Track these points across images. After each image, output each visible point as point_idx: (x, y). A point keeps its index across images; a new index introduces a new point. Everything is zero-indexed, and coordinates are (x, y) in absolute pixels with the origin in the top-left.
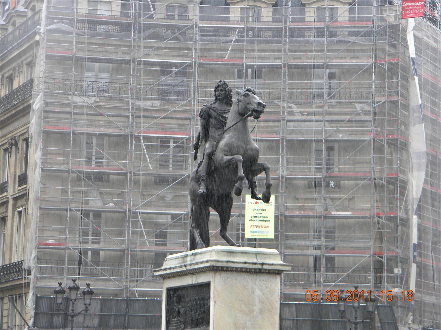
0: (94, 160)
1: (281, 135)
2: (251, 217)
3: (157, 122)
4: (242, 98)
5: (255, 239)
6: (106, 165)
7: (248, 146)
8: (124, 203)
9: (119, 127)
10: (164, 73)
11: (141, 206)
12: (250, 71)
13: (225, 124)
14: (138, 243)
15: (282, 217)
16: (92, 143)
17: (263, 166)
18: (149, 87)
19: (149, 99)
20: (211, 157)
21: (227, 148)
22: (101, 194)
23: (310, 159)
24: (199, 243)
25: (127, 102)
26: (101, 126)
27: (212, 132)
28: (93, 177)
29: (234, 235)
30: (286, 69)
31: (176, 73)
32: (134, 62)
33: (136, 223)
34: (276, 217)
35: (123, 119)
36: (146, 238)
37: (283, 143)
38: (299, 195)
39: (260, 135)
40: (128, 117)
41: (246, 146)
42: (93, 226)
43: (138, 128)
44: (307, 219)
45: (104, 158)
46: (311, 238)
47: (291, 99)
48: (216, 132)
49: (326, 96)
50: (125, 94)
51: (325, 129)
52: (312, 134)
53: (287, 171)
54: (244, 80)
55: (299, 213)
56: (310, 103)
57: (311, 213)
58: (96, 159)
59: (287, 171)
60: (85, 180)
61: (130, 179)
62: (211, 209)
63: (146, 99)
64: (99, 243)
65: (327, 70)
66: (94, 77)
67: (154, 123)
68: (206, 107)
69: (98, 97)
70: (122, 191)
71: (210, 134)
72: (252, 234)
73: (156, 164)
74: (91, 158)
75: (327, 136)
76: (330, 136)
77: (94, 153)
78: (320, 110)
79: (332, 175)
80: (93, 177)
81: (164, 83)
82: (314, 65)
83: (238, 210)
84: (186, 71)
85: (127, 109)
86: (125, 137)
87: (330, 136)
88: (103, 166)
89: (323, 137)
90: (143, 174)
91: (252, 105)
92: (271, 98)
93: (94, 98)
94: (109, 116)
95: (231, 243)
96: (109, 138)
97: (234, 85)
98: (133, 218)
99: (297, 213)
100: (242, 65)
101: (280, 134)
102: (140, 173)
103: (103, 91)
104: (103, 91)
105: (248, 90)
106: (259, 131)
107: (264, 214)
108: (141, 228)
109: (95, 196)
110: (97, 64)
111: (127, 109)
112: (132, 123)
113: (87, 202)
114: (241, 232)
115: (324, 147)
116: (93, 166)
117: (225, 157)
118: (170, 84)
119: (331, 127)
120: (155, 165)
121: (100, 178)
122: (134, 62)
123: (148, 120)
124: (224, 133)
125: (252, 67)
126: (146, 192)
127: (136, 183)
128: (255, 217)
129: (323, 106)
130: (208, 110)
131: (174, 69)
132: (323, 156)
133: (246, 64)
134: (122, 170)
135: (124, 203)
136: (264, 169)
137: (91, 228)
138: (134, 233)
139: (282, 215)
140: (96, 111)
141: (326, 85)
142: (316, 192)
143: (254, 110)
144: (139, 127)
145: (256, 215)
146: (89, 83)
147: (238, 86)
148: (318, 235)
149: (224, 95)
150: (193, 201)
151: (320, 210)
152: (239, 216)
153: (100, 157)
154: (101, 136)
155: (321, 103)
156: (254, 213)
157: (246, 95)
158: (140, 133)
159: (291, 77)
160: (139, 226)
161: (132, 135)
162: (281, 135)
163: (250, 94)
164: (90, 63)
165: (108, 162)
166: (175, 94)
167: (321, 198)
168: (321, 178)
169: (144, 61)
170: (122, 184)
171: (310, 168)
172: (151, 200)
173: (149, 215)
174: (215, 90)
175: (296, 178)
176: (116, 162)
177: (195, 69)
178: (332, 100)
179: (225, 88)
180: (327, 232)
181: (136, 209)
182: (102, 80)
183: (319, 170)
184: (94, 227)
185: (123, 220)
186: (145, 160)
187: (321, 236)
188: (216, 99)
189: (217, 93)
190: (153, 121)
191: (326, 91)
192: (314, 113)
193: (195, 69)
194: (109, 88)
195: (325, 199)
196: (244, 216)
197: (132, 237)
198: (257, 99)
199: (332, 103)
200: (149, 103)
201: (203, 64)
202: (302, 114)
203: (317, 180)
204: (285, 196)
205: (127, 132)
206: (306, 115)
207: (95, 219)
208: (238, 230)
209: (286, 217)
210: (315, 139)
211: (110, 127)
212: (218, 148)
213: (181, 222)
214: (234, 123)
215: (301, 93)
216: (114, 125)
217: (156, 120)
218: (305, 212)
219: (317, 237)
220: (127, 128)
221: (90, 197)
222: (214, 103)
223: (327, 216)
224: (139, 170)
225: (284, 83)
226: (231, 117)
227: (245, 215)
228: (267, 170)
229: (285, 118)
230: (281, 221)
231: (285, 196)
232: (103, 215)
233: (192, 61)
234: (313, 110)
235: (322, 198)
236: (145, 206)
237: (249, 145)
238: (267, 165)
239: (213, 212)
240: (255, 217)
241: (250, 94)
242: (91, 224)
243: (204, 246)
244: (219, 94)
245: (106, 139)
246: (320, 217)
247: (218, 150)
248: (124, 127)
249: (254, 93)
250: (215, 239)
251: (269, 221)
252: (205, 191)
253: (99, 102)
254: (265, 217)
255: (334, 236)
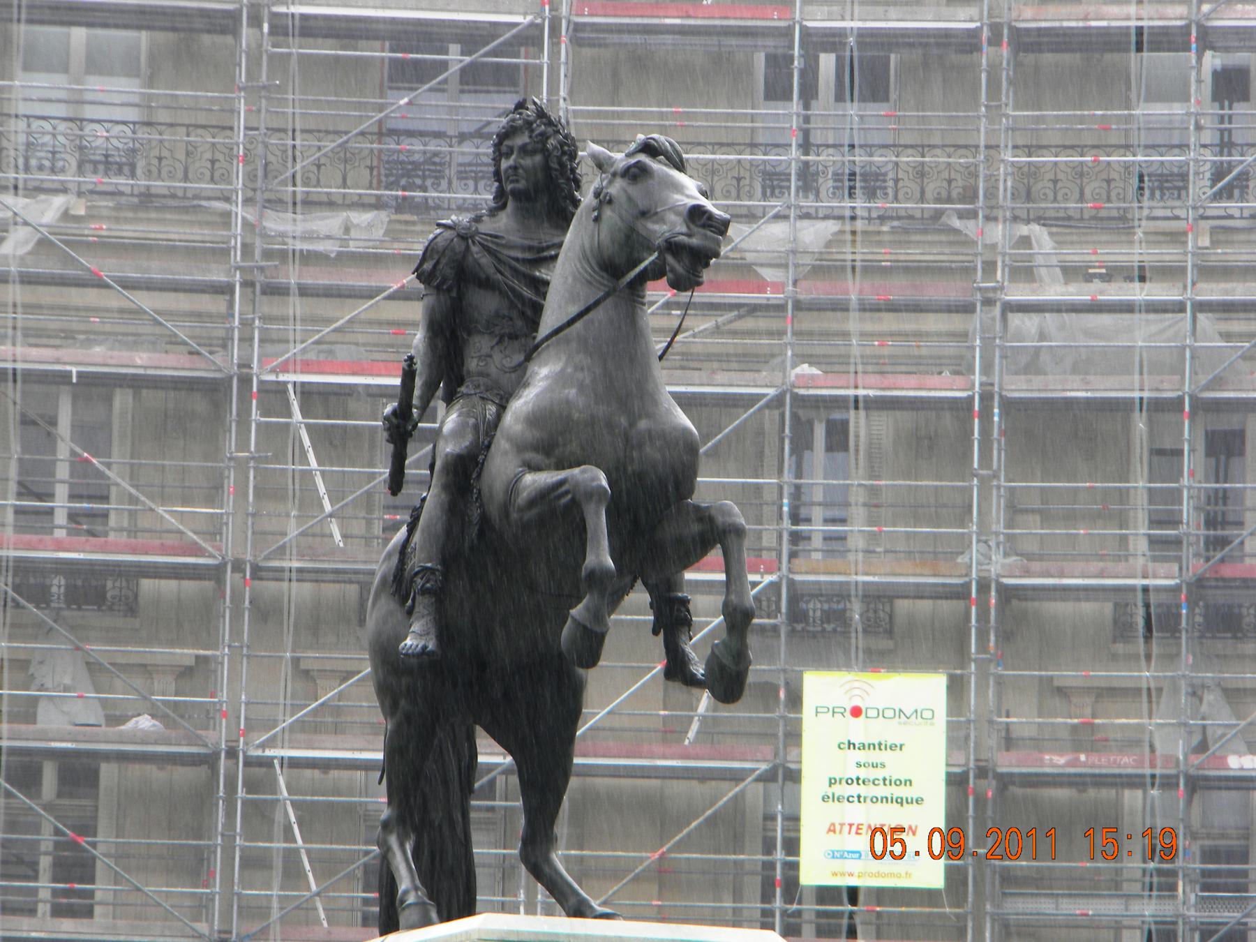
0: (61, 503)
1: (977, 378)
2: (832, 782)
3: (372, 315)
4: (617, 188)
5: (853, 894)
6: (121, 530)
7: (643, 424)
8: (208, 716)
9: (185, 344)
10: (409, 75)
11: (292, 728)
12: (827, 62)
13: (538, 309)
14: (275, 914)
15: (983, 782)
16: (53, 422)
17: (711, 520)
18: (329, 145)
19: (331, 204)
20: (467, 476)
21: (532, 435)
22: (93, 668)
23: (1123, 495)
24: (411, 899)
25: (226, 218)
26: (94, 336)
27: (482, 355)
28: (57, 585)
29: (753, 873)
30: (1005, 52)
31: (464, 71)
32: (255, 21)
33: (260, 815)
34: (956, 782)
35: (206, 303)
36: (314, 887)
37: (986, 415)
38: (1067, 675)
39: (873, 379)
40: (225, 290)
41: (632, 424)
42: (57, 832)
43: (279, 347)
44: (1107, 794)
45: (114, 490)
46: (1127, 888)
47: (1029, 197)
48: (497, 357)
49: (1199, 188)
50: (212, 180)
51: (1194, 350)
52: (1130, 373)
53: (1006, 555)
54: (795, 105)
55: (1068, 764)
56: (1122, 218)
57: (1125, 763)
58: (73, 497)
59: (1006, 555)
60: (17, 605)
61: (237, 598)
62: (479, 731)
63: (310, 204)
64: (88, 913)
65: (1209, 54)
66: (62, 95)
67: (351, 321)
68: (449, 234)
69: (80, 194)
70: (197, 657)
71: (472, 364)
72: (837, 865)
73: (369, 523)
74: (50, 496)
75: (1203, 379)
76: (1217, 383)
77: (63, 471)
78: (1168, 254)
79: (1227, 571)
80: (57, 585)
81: (402, 125)
82: (1140, 31)
83: (767, 750)
84: (517, 66)
85: (223, 253)
86: (214, 390)
87: (1217, 383)
88: (106, 534)
89: (1183, 386)
90: (300, 570)
91: (662, 220)
92: (929, 194)
93: (59, 201)
94: (128, 285)
95: (572, 901)
96: (137, 396)
97: (753, 130)
98: (251, 786)
99: (1056, 762)
100: (787, 33)
101: (971, 370)
102: (286, 564)
103: (107, 164)
104: (107, 164)
105: (649, 149)
106: (865, 360)
107: (895, 765)
108: (289, 837)
109: (67, 681)
110: (79, 35)
111: (223, 253)
112: (246, 324)
113: (26, 712)
114: (779, 855)
115: (1189, 436)
116: (60, 534)
117: (529, 478)
118: (435, 127)
119: (1227, 336)
120: (358, 528)
121: (96, 594)
122: (255, 21)
123: (324, 307)
124: (528, 358)
125: (832, 41)
126: (312, 658)
127: (266, 613)
128: (849, 782)
129: (1185, 234)
130: (459, 246)
131: (455, 57)
132: (1185, 481)
133: (803, 28)
134: (196, 550)
135: (208, 716)
136: (714, 534)
137: (46, 839)
138: (255, 863)
139: (982, 773)
140: (69, 261)
141: (1198, 127)
142: (1148, 657)
143: (672, 247)
144: (280, 341)
145: (854, 773)
146: (36, 124)
147: (601, 136)
148: (1160, 872)
149: (540, 176)
150: (389, 694)
151: (1174, 748)
152: (767, 778)
153: (91, 490)
154: (96, 386)
155: (1177, 218)
156: (847, 764)
157: (636, 174)
158: (284, 368)
159: (1032, 87)
160: (278, 830)
161: (245, 381)
162: (977, 378)
163: (656, 166)
164: (37, 28)
165: (132, 514)
166: (462, 176)
167: (1175, 690)
168: (1176, 590)
169: (304, 17)
170: (197, 621)
171: (1123, 539)
172: (340, 696)
173: (334, 774)
174: (497, 146)
175: (1044, 588)
176: (168, 514)
177: (554, 54)
178: (1232, 206)
179: (544, 137)
180: (1210, 855)
181: (263, 746)
182: (101, 112)
183: (1164, 547)
184: (64, 834)
185: (202, 799)
186: (309, 500)
187: (1173, 873)
188: (501, 196)
189: (505, 164)
190: (349, 312)
191: (1200, 159)
192: (1142, 268)
193: (554, 54)
194: (134, 151)
195: (1196, 693)
196: (794, 777)
197: (245, 884)
198: (689, 190)
199: (1231, 217)
200: (328, 223)
201: (595, 27)
202: (1072, 272)
203: (1153, 599)
204: (1000, 681)
205: (225, 363)
206: (1102, 277)
207: (71, 796)
208: (769, 847)
209: (1005, 781)
210: (1146, 395)
211: (135, 342)
212: (498, 433)
213: (491, 809)
214: (574, 310)
215: (1080, 172)
216: (158, 330)
217: (362, 308)
218: (1094, 759)
219: (1155, 880)
220: (224, 346)
221: (42, 688)
222: (493, 212)
223: (1207, 778)
224: (281, 552)
225: (991, 120)
226: (564, 285)
227: (799, 772)
228: (732, 540)
229: (999, 295)
230: (980, 802)
231: (1000, 681)
232: (107, 772)
233: (540, 14)
234: (1137, 253)
235: (1184, 687)
236: (309, 729)
237: (649, 416)
238: (729, 513)
239: (492, 756)
240: (849, 782)
241: (656, 166)
242: (49, 822)
243: (434, 915)
244: (515, 168)
245: (122, 400)
246: (1168, 783)
247: (501, 444)
248: (208, 343)
249: (680, 166)
250: (655, 889)
251: (919, 801)
252: (431, 646)
253: (90, 217)
254: (898, 783)
255: (1245, 874)
